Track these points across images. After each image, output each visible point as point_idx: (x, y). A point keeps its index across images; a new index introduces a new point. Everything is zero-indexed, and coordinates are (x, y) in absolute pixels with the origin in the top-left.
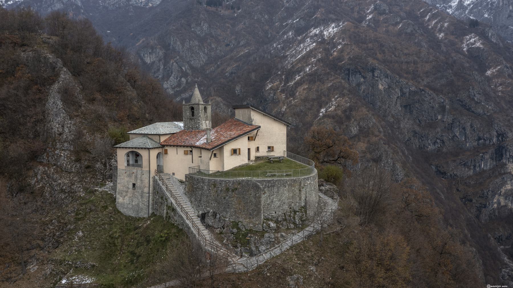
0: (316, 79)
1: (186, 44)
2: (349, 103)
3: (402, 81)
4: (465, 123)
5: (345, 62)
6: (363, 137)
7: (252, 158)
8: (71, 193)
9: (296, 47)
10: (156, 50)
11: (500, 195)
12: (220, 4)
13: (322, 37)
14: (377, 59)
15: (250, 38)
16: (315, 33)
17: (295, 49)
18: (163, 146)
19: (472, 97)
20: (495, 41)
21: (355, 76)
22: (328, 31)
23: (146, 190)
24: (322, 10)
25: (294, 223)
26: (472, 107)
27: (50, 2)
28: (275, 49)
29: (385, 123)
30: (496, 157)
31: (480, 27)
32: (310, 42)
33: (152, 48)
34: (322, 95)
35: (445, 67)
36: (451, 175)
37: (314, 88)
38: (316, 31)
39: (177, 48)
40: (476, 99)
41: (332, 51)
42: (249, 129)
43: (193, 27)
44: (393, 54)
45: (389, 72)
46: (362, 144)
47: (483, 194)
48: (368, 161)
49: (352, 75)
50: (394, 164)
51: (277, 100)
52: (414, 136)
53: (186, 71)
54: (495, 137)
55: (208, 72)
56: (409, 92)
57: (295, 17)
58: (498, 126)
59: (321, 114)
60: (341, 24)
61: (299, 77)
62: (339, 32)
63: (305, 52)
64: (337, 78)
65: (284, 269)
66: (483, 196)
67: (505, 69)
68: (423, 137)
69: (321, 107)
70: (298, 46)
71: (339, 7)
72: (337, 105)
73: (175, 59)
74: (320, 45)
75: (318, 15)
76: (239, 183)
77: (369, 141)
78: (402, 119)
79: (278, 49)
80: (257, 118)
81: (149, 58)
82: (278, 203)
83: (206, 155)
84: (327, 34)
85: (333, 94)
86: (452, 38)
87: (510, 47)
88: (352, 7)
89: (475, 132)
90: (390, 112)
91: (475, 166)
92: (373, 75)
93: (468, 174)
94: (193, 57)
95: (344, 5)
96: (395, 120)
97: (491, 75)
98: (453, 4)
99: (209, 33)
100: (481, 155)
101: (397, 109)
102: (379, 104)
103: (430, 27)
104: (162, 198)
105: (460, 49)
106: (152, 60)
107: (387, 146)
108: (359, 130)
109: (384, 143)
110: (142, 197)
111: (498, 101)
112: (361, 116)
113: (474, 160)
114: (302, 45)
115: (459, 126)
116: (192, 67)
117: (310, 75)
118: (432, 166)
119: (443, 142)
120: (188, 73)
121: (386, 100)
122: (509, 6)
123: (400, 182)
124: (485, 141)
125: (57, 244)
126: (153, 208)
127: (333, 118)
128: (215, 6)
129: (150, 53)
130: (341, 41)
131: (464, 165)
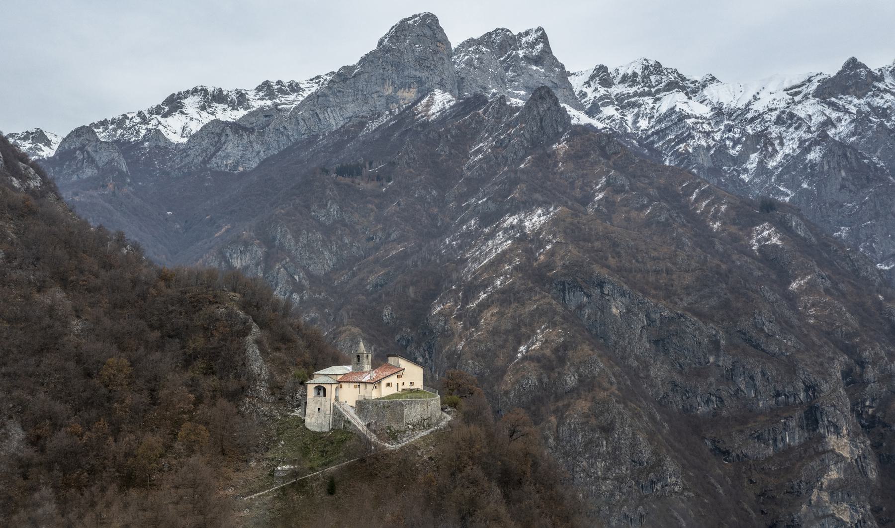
0: (512, 300)
1: (301, 238)
2: (563, 336)
3: (648, 302)
4: (752, 368)
5: (557, 272)
6: (585, 391)
7: (400, 390)
8: (272, 416)
9: (482, 246)
10: (252, 247)
11: (821, 489)
12: (359, 173)
13: (522, 231)
14: (608, 267)
15: (407, 228)
16: (511, 223)
17: (480, 249)
18: (339, 382)
19: (760, 327)
20: (802, 234)
21: (574, 293)
22: (531, 220)
23: (328, 412)
24: (523, 186)
25: (424, 426)
26: (762, 343)
27: (76, 166)
28: (447, 247)
29: (620, 369)
30: (807, 425)
31: (778, 212)
32: (503, 237)
33: (246, 244)
34: (521, 324)
35: (715, 280)
36: (738, 456)
37: (508, 313)
38: (512, 220)
39: (286, 244)
40: (766, 329)
41: (537, 254)
42: (398, 370)
43: (314, 211)
44: (634, 258)
45: (626, 287)
46: (583, 402)
47: (792, 487)
48: (593, 430)
49: (569, 293)
50: (633, 434)
51: (450, 332)
52: (672, 390)
53: (300, 281)
54: (802, 390)
55: (336, 283)
56: (661, 319)
57: (481, 194)
58: (804, 374)
59: (519, 355)
60: (551, 209)
61: (485, 295)
62: (547, 223)
63: (494, 255)
64: (545, 297)
65: (415, 447)
66: (792, 491)
67: (819, 280)
68: (687, 392)
69: (519, 344)
70: (484, 244)
71: (550, 181)
72: (544, 339)
73: (284, 262)
74: (519, 244)
75: (516, 194)
76: (391, 403)
77: (594, 398)
78: (652, 362)
79: (452, 248)
80: (403, 363)
81: (239, 261)
82: (414, 414)
83: (370, 387)
84: (530, 226)
85: (538, 323)
86: (733, 229)
87: (829, 243)
88: (571, 180)
89: (769, 384)
90: (632, 351)
91: (775, 440)
92: (602, 292)
93: (765, 454)
94: (312, 258)
95: (558, 177)
96: (641, 365)
97: (797, 289)
98: (749, 167)
99: (340, 219)
100: (783, 421)
101: (642, 346)
102: (613, 337)
103: (698, 212)
104: (340, 416)
105: (747, 247)
106: (244, 264)
107: (621, 406)
108: (580, 381)
109: (617, 401)
110: (325, 417)
111: (806, 332)
112: (582, 358)
113: (773, 430)
114: (490, 243)
115: (744, 372)
116: (310, 276)
117: (503, 292)
118: (707, 441)
119: (721, 400)
120: (303, 286)
121: (624, 331)
122: (840, 171)
123: (645, 464)
124: (788, 398)
125: (267, 449)
126: (332, 425)
127: (538, 360)
128: (351, 176)
129: (241, 252)
130: (551, 237)
131: (758, 437)
